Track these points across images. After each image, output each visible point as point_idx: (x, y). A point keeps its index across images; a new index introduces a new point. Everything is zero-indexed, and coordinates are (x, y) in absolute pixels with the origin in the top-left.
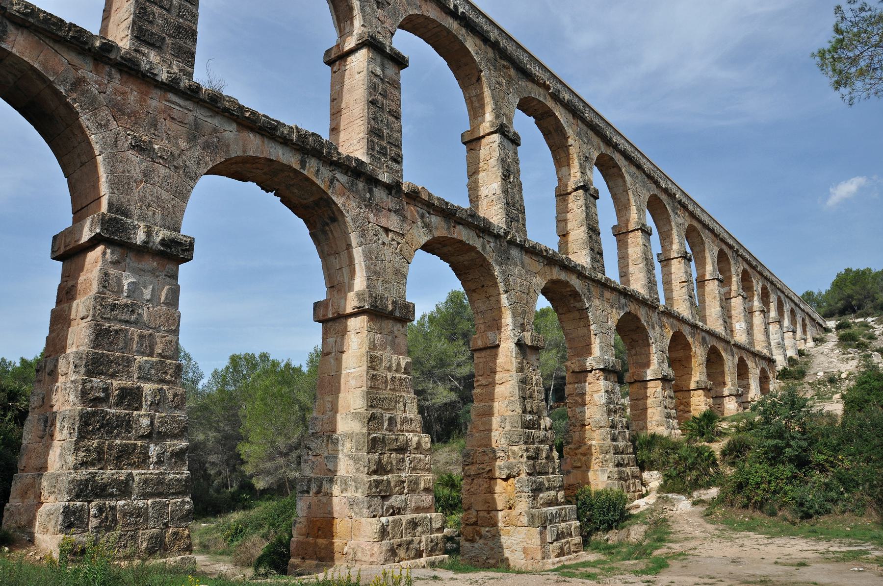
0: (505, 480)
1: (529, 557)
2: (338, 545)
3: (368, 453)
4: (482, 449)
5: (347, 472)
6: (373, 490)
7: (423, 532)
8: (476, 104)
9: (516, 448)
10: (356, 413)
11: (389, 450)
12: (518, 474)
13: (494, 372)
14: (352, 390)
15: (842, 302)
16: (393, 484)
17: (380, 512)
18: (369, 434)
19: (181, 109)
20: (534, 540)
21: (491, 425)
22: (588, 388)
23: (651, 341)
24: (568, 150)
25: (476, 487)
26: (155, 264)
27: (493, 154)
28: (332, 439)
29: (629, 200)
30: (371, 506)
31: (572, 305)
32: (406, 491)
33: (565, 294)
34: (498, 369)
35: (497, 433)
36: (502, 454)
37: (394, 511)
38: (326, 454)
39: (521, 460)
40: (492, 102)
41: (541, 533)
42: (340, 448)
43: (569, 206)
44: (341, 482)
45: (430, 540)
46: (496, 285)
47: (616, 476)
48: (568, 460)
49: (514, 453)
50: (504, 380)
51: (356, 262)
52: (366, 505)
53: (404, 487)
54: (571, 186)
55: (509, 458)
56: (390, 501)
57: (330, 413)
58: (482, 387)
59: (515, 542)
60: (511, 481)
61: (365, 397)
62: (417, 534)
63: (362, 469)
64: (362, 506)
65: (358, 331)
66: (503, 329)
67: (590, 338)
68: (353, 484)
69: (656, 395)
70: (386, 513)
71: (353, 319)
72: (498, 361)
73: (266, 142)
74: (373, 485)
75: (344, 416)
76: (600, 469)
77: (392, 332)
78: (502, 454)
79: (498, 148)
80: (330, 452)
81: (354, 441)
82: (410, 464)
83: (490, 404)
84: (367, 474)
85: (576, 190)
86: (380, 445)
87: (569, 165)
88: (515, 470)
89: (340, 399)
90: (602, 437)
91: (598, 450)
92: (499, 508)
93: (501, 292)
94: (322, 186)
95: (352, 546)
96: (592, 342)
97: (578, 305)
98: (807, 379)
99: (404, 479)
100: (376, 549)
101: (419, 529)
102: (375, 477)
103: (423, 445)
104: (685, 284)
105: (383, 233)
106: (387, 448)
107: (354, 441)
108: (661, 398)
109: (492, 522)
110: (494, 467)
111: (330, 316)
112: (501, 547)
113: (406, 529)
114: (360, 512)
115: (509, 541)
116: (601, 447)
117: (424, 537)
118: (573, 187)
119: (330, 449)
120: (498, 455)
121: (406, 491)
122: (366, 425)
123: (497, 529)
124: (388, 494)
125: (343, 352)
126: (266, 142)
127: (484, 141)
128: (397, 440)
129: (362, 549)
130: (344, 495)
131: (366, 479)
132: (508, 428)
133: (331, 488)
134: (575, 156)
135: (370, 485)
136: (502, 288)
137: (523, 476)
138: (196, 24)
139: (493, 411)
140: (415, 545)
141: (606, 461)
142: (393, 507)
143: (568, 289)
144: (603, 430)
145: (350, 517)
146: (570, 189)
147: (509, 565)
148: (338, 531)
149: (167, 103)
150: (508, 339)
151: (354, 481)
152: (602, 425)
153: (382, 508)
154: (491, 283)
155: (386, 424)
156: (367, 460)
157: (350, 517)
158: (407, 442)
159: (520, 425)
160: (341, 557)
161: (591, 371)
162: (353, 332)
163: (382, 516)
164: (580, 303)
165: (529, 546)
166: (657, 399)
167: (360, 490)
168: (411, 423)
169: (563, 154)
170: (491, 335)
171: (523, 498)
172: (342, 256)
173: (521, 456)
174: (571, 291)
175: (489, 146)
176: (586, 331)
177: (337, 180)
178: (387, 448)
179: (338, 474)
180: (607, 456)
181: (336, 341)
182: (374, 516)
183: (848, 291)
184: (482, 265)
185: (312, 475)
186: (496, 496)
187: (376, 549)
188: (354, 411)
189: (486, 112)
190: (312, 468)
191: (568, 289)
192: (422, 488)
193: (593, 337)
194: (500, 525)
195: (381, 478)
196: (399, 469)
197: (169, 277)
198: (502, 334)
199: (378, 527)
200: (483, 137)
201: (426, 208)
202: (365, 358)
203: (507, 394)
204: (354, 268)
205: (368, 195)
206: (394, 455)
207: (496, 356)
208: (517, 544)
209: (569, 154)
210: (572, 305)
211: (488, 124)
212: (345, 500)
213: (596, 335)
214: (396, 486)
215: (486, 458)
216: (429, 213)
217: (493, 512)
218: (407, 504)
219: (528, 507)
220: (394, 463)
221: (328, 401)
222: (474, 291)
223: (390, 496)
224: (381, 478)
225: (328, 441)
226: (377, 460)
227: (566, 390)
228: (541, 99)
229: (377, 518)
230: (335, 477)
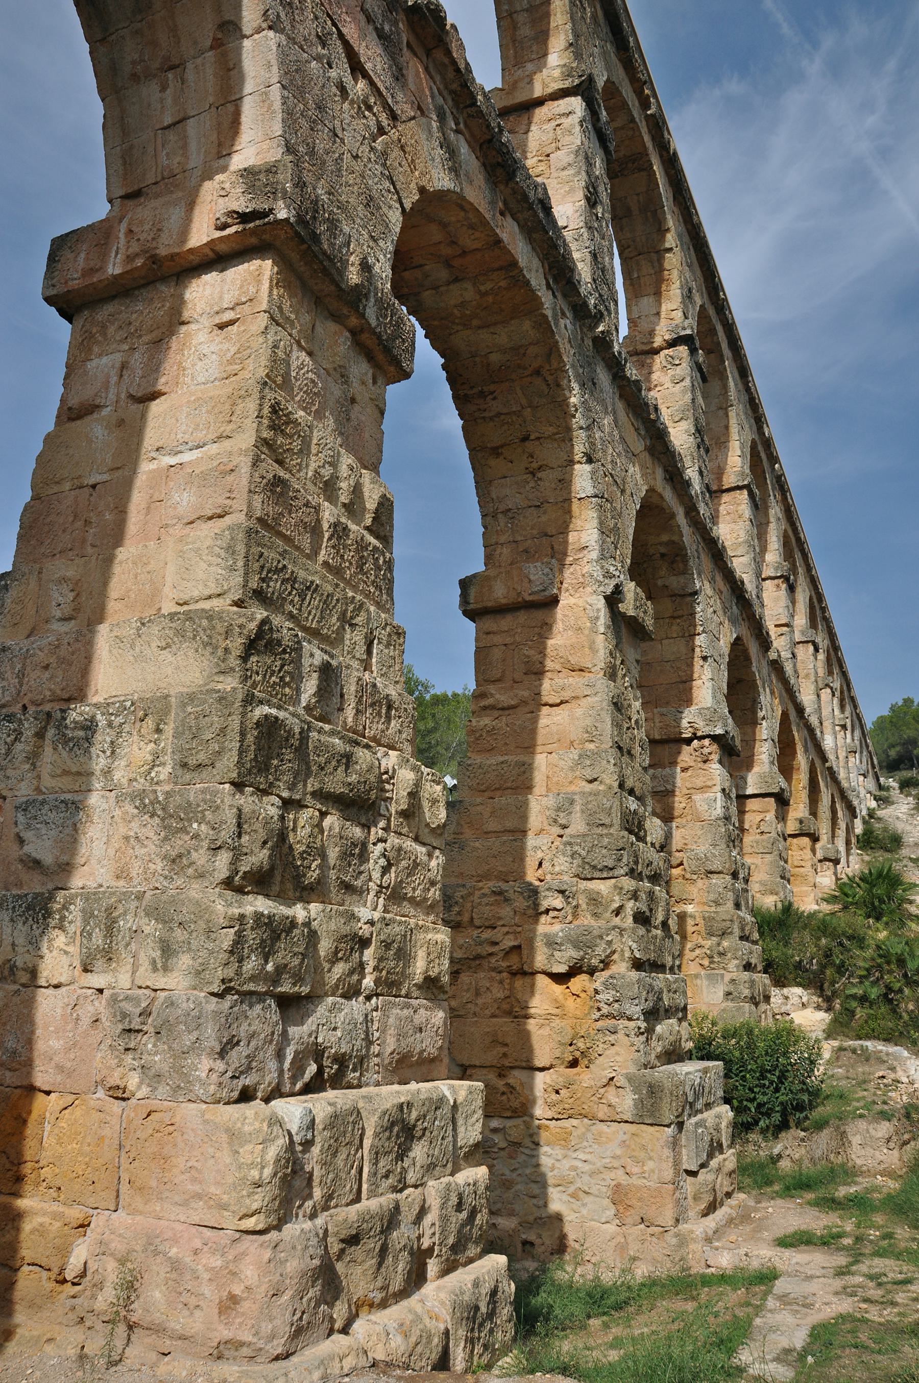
0: (560, 979)
1: (632, 1217)
2: (40, 1231)
3: (238, 786)
4: (492, 885)
6: (251, 965)
7: (430, 1168)
8: (525, 31)
9: (602, 887)
11: (319, 795)
12: (606, 963)
13: (537, 672)
14: (178, 530)
15: (898, 749)
16: (325, 946)
17: (271, 1077)
18: (249, 700)
20: (650, 1165)
21: (524, 818)
22: (681, 780)
23: (761, 714)
24: (660, 260)
25: (467, 996)
27: (566, 140)
28: (61, 724)
29: (727, 427)
30: (232, 1043)
31: (660, 583)
32: (368, 982)
33: (652, 551)
34: (549, 664)
35: (543, 841)
36: (558, 902)
37: (320, 1070)
38: (24, 791)
39: (617, 921)
40: (569, 26)
41: (675, 1144)
42: (100, 763)
43: (654, 377)
44: (88, 915)
45: (454, 1200)
46: (565, 436)
47: (747, 992)
49: (594, 900)
50: (566, 695)
51: (249, 87)
52: (211, 1036)
53: (362, 966)
54: (662, 334)
55: (575, 915)
56: (310, 1024)
57: (64, 628)
58: (496, 713)
59: (587, 1167)
60: (579, 982)
61: (241, 548)
62: (411, 1178)
63: (200, 857)
64: (188, 1040)
65: (228, 316)
66: (569, 559)
67: (691, 665)
68: (150, 927)
69: (762, 828)
70: (294, 1079)
71: (211, 278)
72: (550, 642)
74: (252, 938)
75: (128, 632)
76: (703, 972)
78: (558, 902)
79: (578, 128)
80: (48, 782)
81: (169, 730)
82: (385, 870)
83: (522, 758)
84: (228, 883)
85: (672, 344)
86: (287, 763)
87: (658, 294)
89: (117, 569)
90: (712, 896)
91: (702, 927)
92: (539, 1063)
93: (577, 458)
95: (117, 1246)
96: (696, 676)
97: (674, 582)
98: (904, 852)
99: (365, 931)
100: (250, 1273)
101: (419, 1152)
102: (261, 904)
103: (426, 805)
104: (785, 629)
106: (312, 784)
108: (774, 834)
109: (515, 1104)
110: (531, 941)
112: (541, 1182)
113: (377, 1155)
114: (177, 1069)
115: (566, 1164)
116: (708, 920)
117: (434, 1189)
118: (667, 337)
119: (45, 769)
120: (545, 904)
121: (368, 982)
122: (233, 661)
123: (528, 1125)
124: (305, 990)
125: (155, 395)
127: (541, 113)
128: (347, 760)
129: (176, 1266)
130: (97, 980)
131: (220, 907)
132: (578, 825)
133: (34, 944)
134: (675, 274)
135: (239, 940)
136: (579, 449)
137: (621, 968)
139: (531, 779)
140: (401, 1235)
141: (721, 954)
142: (317, 1052)
144: (715, 880)
145: (119, 1094)
146: (658, 342)
147: (563, 1237)
148: (46, 1157)
150: (583, 585)
151: (154, 912)
152: (714, 868)
153: (280, 1055)
154: (551, 430)
155: (310, 686)
156: (230, 817)
157: (119, 1094)
158: (384, 778)
159: (617, 821)
160: (51, 1296)
161: (688, 741)
162: (207, 322)
163: (276, 1093)
164: (682, 579)
165: (635, 1181)
166: (765, 836)
167: (185, 961)
168: (389, 718)
169: (646, 269)
170: (536, 572)
171: (620, 1035)
173: (618, 912)
175: (554, 123)
176: (683, 650)
178: (312, 784)
179: (77, 881)
180: (725, 944)
181: (124, 366)
182: (246, 1096)
183: (909, 733)
184: (537, 372)
186: (532, 1025)
187: (250, 1273)
189: (551, 50)
192: (419, 978)
193: (698, 662)
194: (539, 1111)
195: (284, 910)
196: (348, 887)
198: (567, 573)
199: (272, 1152)
200: (540, 102)
202: (251, 406)
203: (575, 733)
204: (237, 114)
206: (332, 821)
207: (546, 628)
208: (592, 1174)
209: (662, 269)
210: (660, 583)
211: (557, 73)
212: (100, 1005)
213: (705, 658)
214: (334, 959)
215: (506, 911)
217: (516, 1073)
218: (369, 1042)
219: (635, 1061)
220: (333, 854)
221: (64, 580)
222: (496, 452)
223: (313, 998)
224: (284, 910)
225: (40, 735)
226: (277, 826)
229: (257, 1104)
230: (60, 896)
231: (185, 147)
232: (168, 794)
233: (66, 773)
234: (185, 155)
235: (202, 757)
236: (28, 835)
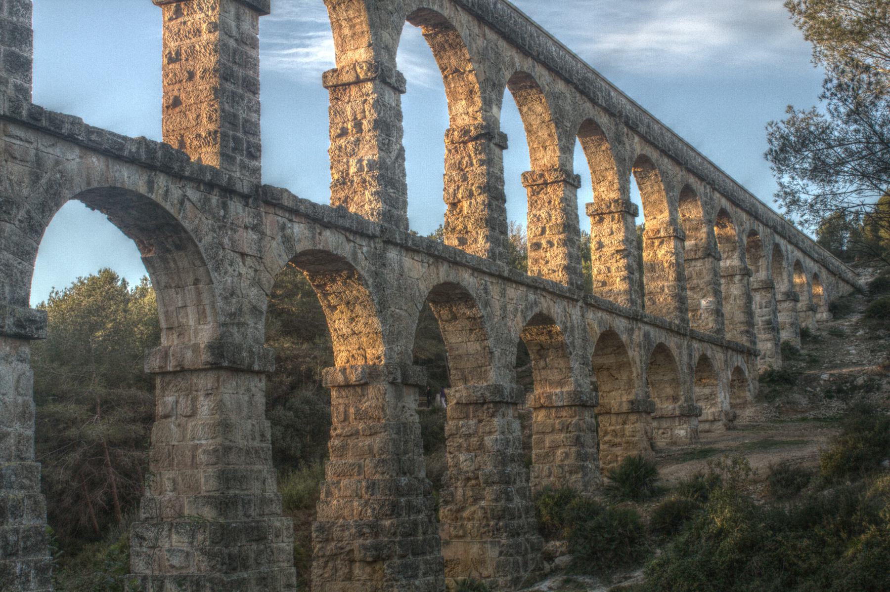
5: (199, 570)
10: (209, 497)
19: (21, 143)
26: (8, 348)
48: (446, 526)
65: (210, 392)
68: (208, 584)
73: (110, 162)
77: (248, 390)
80: (174, 544)
81: (208, 532)
88: (385, 552)
94: (172, 211)
105: (239, 260)
107: (208, 532)
111: (170, 368)
126: (110, 162)
138: (30, 18)
141: (497, 530)
143: (458, 291)
149: (7, 139)
172: (186, 291)
174: (461, 293)
177: (189, 199)
181: (177, 402)
185: (148, 572)
188: (205, 494)
190: (148, 563)
191: (458, 291)
197: (21, 361)
201: (287, 215)
205: (222, 213)
216: (291, 221)
225: (170, 530)
227: (447, 428)
228: (436, 8)
231: (187, 316)
232: (209, 549)
233: (179, 542)
234: (188, 319)
235: (217, 540)
236: (171, 559)
